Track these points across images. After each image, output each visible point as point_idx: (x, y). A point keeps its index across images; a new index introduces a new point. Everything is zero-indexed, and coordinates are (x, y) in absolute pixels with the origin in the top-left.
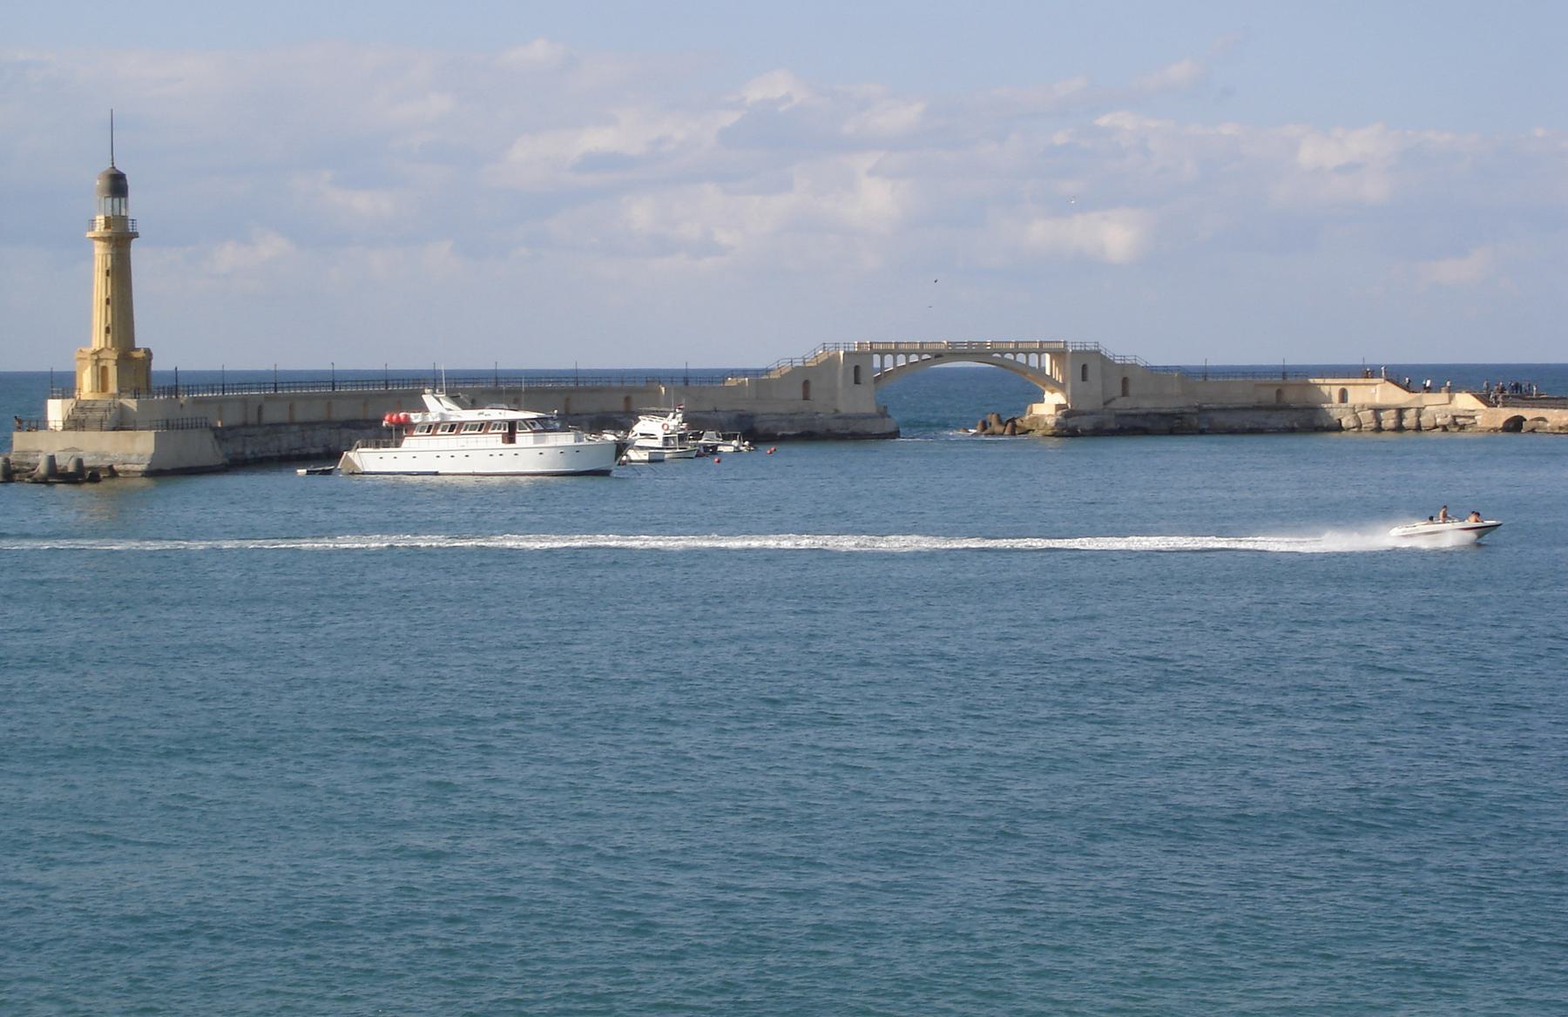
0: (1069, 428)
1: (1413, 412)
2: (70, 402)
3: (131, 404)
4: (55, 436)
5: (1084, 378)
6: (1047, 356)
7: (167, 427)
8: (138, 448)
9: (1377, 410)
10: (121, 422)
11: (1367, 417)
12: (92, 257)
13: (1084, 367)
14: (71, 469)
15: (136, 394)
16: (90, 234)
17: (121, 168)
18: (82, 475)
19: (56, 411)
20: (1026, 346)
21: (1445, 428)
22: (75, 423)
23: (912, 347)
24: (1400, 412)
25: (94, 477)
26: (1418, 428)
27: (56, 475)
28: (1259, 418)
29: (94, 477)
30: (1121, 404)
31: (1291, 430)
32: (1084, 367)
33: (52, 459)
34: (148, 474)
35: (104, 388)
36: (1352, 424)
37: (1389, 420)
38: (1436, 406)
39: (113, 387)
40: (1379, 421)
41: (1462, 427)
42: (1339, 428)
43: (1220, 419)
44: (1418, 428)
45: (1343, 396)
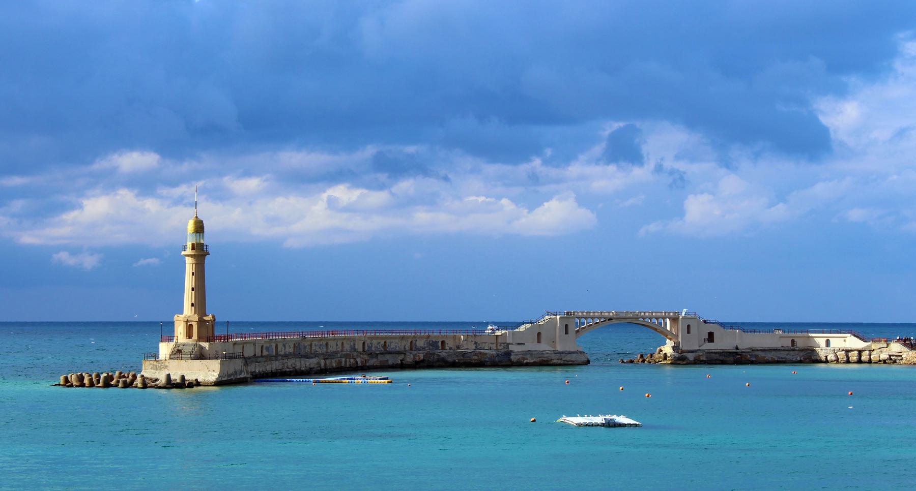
0: (680, 360)
1: (867, 352)
2: (172, 345)
3: (206, 345)
4: (166, 364)
5: (567, 333)
6: (668, 320)
7: (226, 358)
8: (208, 371)
9: (847, 352)
10: (201, 355)
11: (841, 355)
12: (596, 415)
13: (689, 326)
14: (178, 381)
15: (208, 340)
16: (183, 253)
17: (200, 218)
18: (183, 384)
19: (165, 349)
20: (657, 314)
21: (885, 362)
22: (177, 354)
23: (646, 314)
24: (860, 352)
25: (191, 385)
26: (870, 362)
27: (170, 384)
28: (783, 355)
29: (191, 385)
30: (709, 346)
31: (800, 362)
32: (689, 326)
33: (169, 376)
34: (217, 384)
35: (189, 336)
36: (834, 358)
37: (854, 357)
38: (881, 351)
39: (195, 336)
40: (848, 357)
41: (895, 362)
42: (827, 361)
43: (769, 356)
44: (870, 362)
45: (828, 343)
